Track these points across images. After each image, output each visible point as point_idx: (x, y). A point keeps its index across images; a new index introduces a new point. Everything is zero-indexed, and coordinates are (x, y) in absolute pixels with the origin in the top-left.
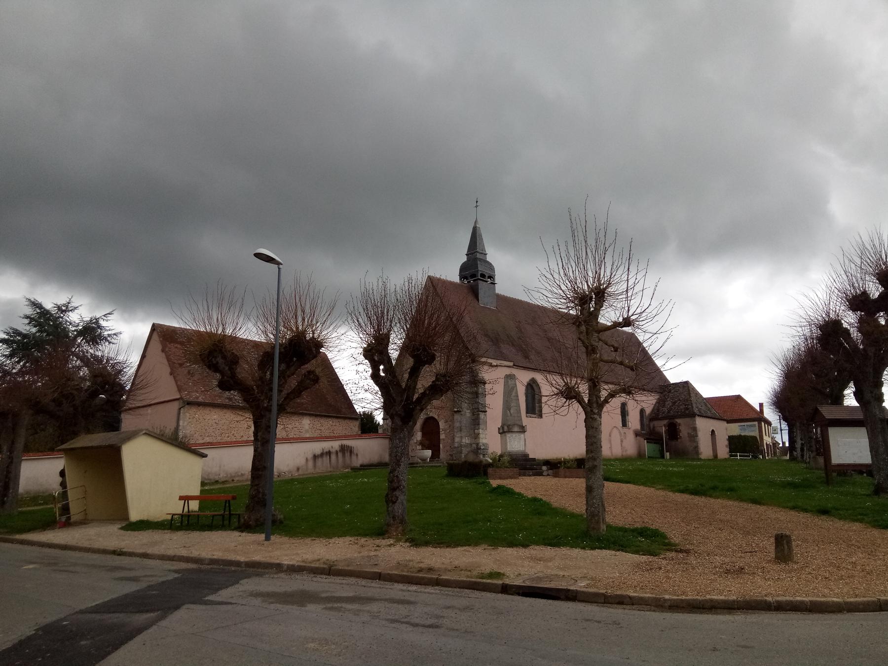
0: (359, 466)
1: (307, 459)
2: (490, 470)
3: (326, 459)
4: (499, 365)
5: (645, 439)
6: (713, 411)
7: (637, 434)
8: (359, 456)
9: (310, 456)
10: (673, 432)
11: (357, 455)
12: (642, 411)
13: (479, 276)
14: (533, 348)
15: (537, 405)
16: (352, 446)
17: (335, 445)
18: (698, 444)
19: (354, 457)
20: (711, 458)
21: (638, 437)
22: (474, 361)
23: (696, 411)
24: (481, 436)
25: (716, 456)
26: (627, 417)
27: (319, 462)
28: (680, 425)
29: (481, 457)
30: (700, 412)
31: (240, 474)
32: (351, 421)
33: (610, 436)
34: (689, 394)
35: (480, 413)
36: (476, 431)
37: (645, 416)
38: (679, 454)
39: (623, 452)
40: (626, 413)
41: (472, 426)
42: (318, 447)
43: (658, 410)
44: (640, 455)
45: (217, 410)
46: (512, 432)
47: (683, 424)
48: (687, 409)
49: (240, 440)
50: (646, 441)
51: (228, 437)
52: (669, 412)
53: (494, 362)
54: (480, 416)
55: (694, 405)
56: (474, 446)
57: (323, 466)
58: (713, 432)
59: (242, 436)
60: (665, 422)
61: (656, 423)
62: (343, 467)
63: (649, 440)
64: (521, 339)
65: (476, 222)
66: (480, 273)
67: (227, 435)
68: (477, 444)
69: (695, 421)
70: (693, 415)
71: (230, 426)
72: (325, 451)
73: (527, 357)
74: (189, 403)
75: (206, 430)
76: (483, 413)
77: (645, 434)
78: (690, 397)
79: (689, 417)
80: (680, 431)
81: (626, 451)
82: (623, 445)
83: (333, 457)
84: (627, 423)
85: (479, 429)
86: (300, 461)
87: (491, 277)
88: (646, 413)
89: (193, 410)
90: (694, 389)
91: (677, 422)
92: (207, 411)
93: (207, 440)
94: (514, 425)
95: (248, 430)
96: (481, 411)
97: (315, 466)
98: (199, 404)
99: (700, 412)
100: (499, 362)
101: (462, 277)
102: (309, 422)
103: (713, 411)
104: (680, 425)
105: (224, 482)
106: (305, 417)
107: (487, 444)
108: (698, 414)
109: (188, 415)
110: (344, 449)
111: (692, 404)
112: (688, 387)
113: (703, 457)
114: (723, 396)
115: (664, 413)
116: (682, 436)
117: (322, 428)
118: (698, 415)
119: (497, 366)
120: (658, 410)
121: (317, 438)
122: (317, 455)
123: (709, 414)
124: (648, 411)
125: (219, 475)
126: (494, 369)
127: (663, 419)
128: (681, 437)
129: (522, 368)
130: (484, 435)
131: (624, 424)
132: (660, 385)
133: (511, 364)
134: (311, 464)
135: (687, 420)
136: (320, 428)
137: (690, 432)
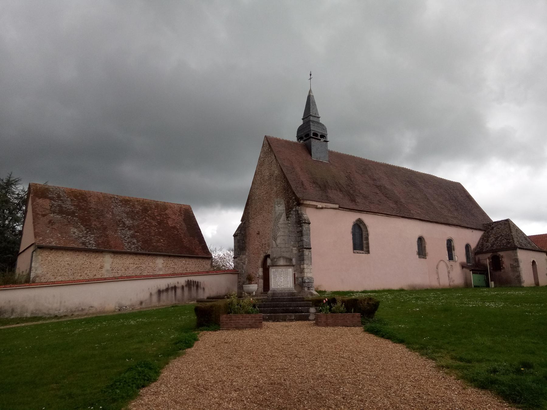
0: (205, 298)
1: (151, 294)
2: (224, 318)
3: (171, 294)
4: (324, 207)
5: (470, 271)
6: (533, 244)
7: (463, 266)
8: (206, 290)
9: (154, 291)
10: (497, 263)
11: (204, 289)
12: (467, 247)
13: (312, 135)
14: (361, 193)
15: (364, 242)
16: (199, 281)
17: (182, 281)
18: (520, 273)
19: (200, 291)
20: (533, 286)
21: (464, 269)
22: (299, 204)
23: (517, 244)
24: (306, 270)
25: (537, 284)
26: (453, 252)
27: (164, 296)
28: (502, 257)
29: (306, 290)
30: (521, 245)
31: (80, 309)
32: (190, 260)
33: (437, 268)
34: (510, 230)
35: (304, 250)
36: (302, 266)
37: (470, 251)
38: (503, 283)
39: (450, 282)
40: (452, 248)
41: (299, 262)
42: (163, 283)
43: (482, 245)
44: (467, 285)
45: (130, 256)
46: (276, 266)
47: (506, 258)
48: (509, 243)
49: (93, 278)
50: (471, 272)
51: (81, 276)
52: (492, 246)
53: (320, 205)
54: (305, 252)
55: (515, 240)
56: (300, 279)
57: (168, 299)
58: (534, 262)
59: (95, 275)
60: (489, 255)
61: (481, 256)
62: (189, 300)
63: (474, 272)
64: (350, 186)
65: (310, 91)
66: (312, 132)
67: (80, 274)
68: (303, 278)
69: (516, 253)
70: (515, 248)
71: (83, 266)
72: (170, 286)
73: (353, 200)
74: (41, 247)
75: (58, 270)
76: (308, 250)
77: (471, 266)
78: (511, 232)
79: (511, 250)
80: (503, 263)
81: (453, 281)
82: (450, 277)
83: (179, 291)
84: (454, 257)
85: (304, 264)
86: (144, 296)
87: (323, 136)
88: (471, 248)
89: (46, 253)
90: (514, 225)
91: (500, 255)
92: (59, 253)
93: (59, 279)
94: (280, 257)
95: (101, 269)
96: (305, 248)
97: (159, 300)
98: (51, 248)
99: (521, 245)
100: (324, 205)
101: (299, 138)
102: (163, 262)
103: (533, 244)
104: (503, 257)
105: (61, 317)
106: (159, 258)
107: (312, 278)
108: (519, 247)
109: (40, 257)
110: (189, 284)
111: (513, 238)
112: (509, 224)
113: (525, 284)
114: (542, 234)
115: (487, 247)
116: (505, 267)
117: (176, 267)
118: (520, 248)
119: (322, 208)
120: (482, 245)
121: (112, 278)
122: (161, 289)
123: (529, 246)
124: (473, 246)
125: (60, 310)
126: (318, 211)
127: (487, 253)
128: (504, 267)
129: (349, 210)
130: (309, 270)
131: (451, 257)
132: (483, 224)
133: (337, 206)
134: (155, 298)
135: (510, 252)
136: (173, 267)
137: (512, 263)
